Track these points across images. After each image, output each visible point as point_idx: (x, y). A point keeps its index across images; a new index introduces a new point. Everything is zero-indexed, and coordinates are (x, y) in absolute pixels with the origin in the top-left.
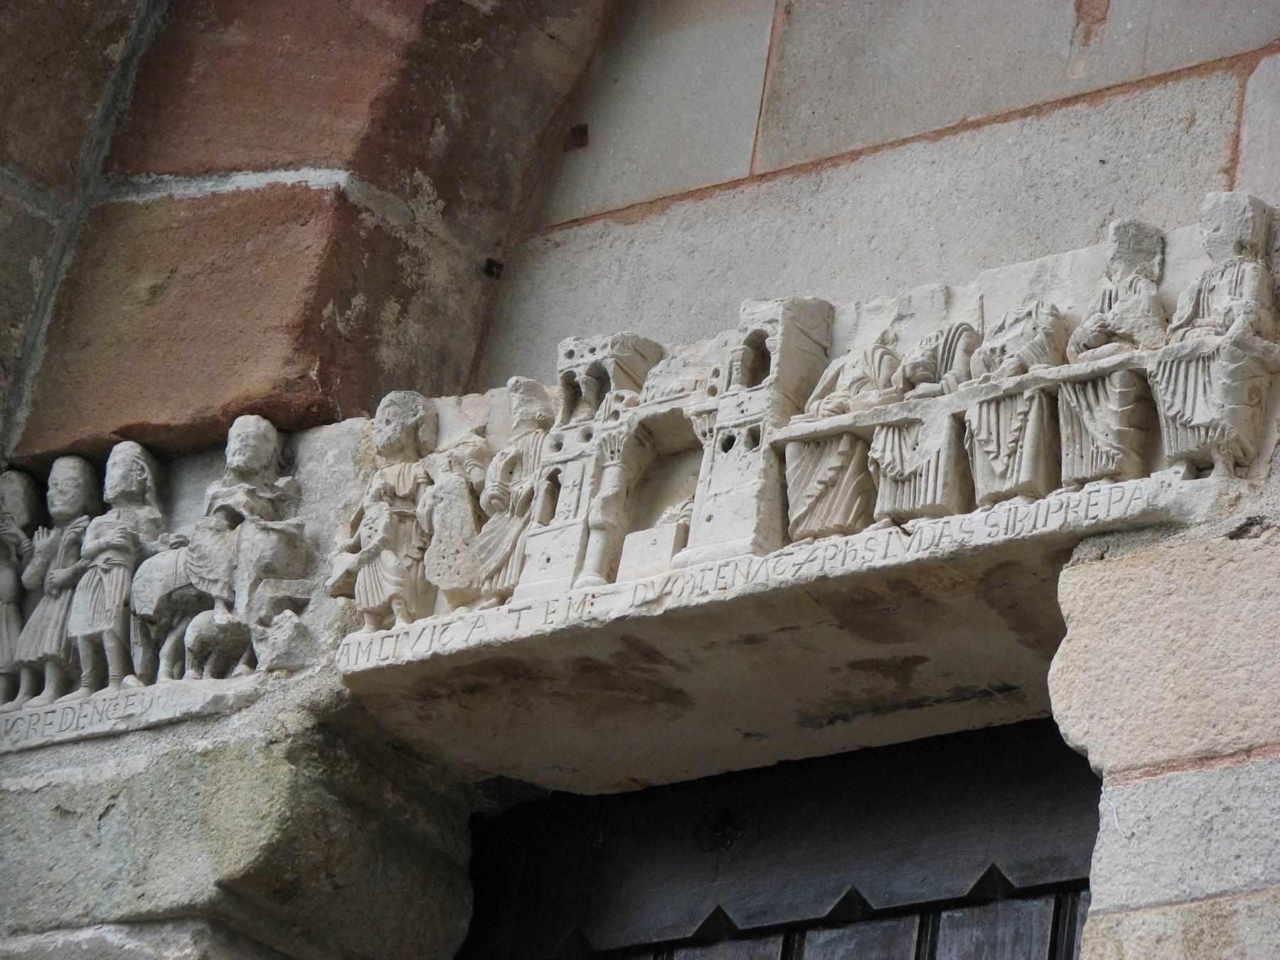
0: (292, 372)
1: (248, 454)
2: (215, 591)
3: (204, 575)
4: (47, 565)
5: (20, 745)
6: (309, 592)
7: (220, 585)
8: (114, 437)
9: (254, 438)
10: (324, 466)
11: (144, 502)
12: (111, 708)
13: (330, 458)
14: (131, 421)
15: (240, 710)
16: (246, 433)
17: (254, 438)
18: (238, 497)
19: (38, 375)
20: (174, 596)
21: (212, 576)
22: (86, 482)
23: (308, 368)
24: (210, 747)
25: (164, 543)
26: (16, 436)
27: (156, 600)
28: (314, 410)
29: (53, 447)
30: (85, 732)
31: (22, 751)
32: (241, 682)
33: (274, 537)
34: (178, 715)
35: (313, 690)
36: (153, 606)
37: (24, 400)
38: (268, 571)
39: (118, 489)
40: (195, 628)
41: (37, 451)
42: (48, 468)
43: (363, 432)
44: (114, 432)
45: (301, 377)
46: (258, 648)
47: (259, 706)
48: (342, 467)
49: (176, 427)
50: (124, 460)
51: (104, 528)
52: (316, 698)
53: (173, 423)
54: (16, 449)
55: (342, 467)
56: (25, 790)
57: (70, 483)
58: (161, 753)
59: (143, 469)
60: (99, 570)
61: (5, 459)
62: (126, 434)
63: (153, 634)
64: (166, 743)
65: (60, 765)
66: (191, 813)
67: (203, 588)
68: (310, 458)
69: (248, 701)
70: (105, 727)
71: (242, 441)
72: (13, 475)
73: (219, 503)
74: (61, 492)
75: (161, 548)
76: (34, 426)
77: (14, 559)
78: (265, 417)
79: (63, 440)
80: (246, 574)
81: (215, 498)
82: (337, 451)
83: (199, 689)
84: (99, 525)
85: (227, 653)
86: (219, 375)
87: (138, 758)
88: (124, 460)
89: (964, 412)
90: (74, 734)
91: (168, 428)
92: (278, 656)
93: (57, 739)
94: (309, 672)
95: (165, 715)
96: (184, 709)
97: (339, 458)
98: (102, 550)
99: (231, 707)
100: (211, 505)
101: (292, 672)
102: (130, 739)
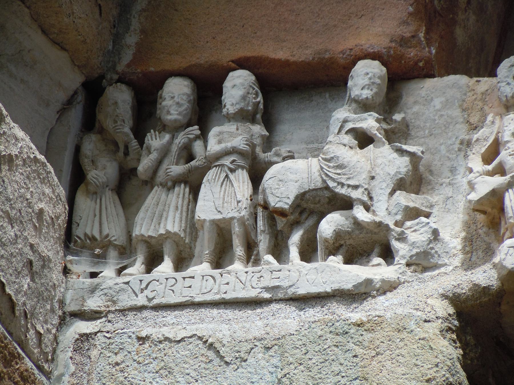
0: (407, 31)
1: (375, 90)
2: (355, 194)
3: (343, 181)
4: (160, 162)
5: (155, 302)
6: (432, 206)
7: (360, 190)
8: (233, 65)
9: (379, 78)
10: (432, 109)
11: (253, 121)
12: (255, 279)
13: (437, 103)
14: (249, 54)
15: (384, 293)
16: (366, 77)
17: (379, 78)
18: (370, 122)
19: (144, 10)
20: (307, 196)
21: (352, 182)
22: (194, 99)
23: (417, 31)
24: (365, 319)
25: (277, 155)
26: (127, 57)
27: (292, 197)
28: (421, 64)
29: (168, 67)
30: (228, 297)
31: (158, 308)
32: (377, 270)
33: (406, 160)
34: (329, 290)
35: (455, 284)
36: (290, 202)
37: (132, 28)
38: (400, 185)
39: (238, 107)
40: (330, 224)
41: (152, 69)
42: (160, 85)
43: (468, 87)
44: (233, 61)
45: (413, 37)
46: (395, 244)
47: (401, 290)
48: (450, 112)
49: (295, 63)
50: (238, 87)
51: (226, 136)
52: (459, 291)
53: (292, 59)
54: (128, 66)
55: (450, 112)
56: (167, 339)
57: (185, 97)
58: (312, 319)
59: (257, 94)
60: (226, 169)
61: (117, 73)
62: (241, 64)
63: (291, 225)
64: (313, 313)
65: (202, 321)
66: (350, 372)
67: (343, 191)
68: (416, 102)
69: (389, 287)
70: (252, 294)
71: (370, 79)
72: (124, 87)
73: (350, 126)
74: (178, 103)
75: (275, 159)
76: (142, 52)
77: (121, 154)
78: (383, 64)
79: (179, 62)
80: (384, 185)
81: (345, 121)
82: (443, 99)
83: (336, 273)
84: (221, 133)
85: (368, 244)
86: (335, 26)
87: (287, 320)
88: (238, 87)
89: (475, 192)
90: (217, 297)
91: (287, 63)
92: (417, 254)
93: (197, 299)
94: (443, 270)
95: (314, 290)
96: (336, 286)
97: (447, 104)
98: (227, 153)
99: (378, 291)
100: (342, 127)
101: (425, 269)
102: (274, 306)
